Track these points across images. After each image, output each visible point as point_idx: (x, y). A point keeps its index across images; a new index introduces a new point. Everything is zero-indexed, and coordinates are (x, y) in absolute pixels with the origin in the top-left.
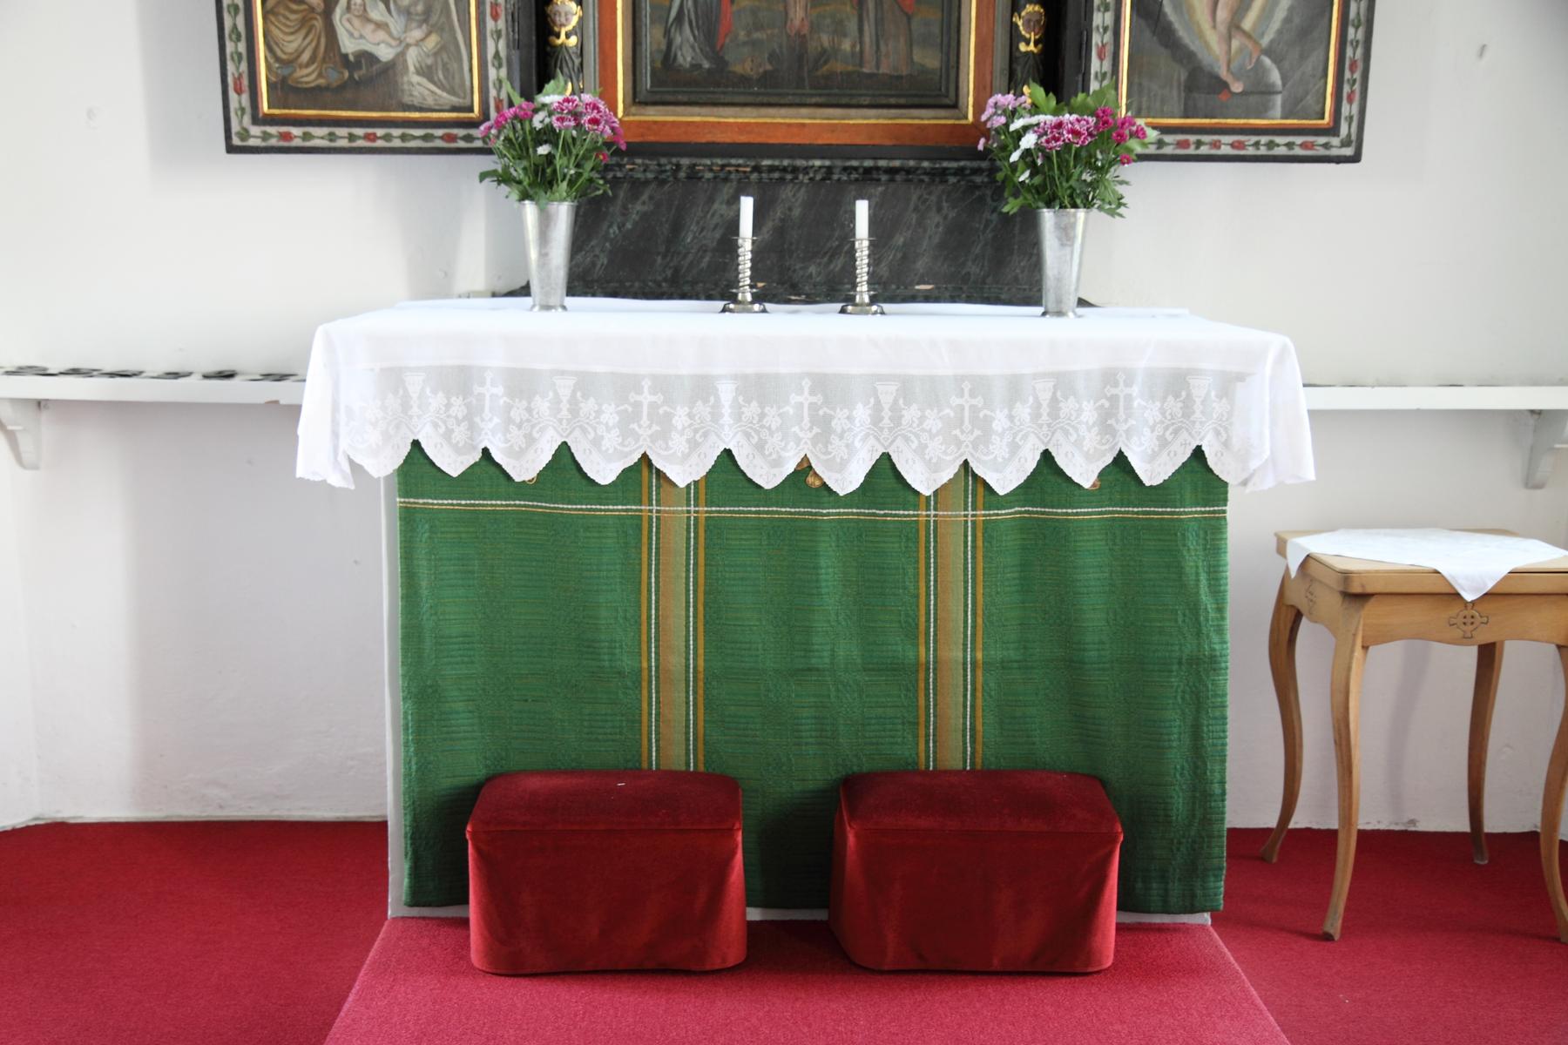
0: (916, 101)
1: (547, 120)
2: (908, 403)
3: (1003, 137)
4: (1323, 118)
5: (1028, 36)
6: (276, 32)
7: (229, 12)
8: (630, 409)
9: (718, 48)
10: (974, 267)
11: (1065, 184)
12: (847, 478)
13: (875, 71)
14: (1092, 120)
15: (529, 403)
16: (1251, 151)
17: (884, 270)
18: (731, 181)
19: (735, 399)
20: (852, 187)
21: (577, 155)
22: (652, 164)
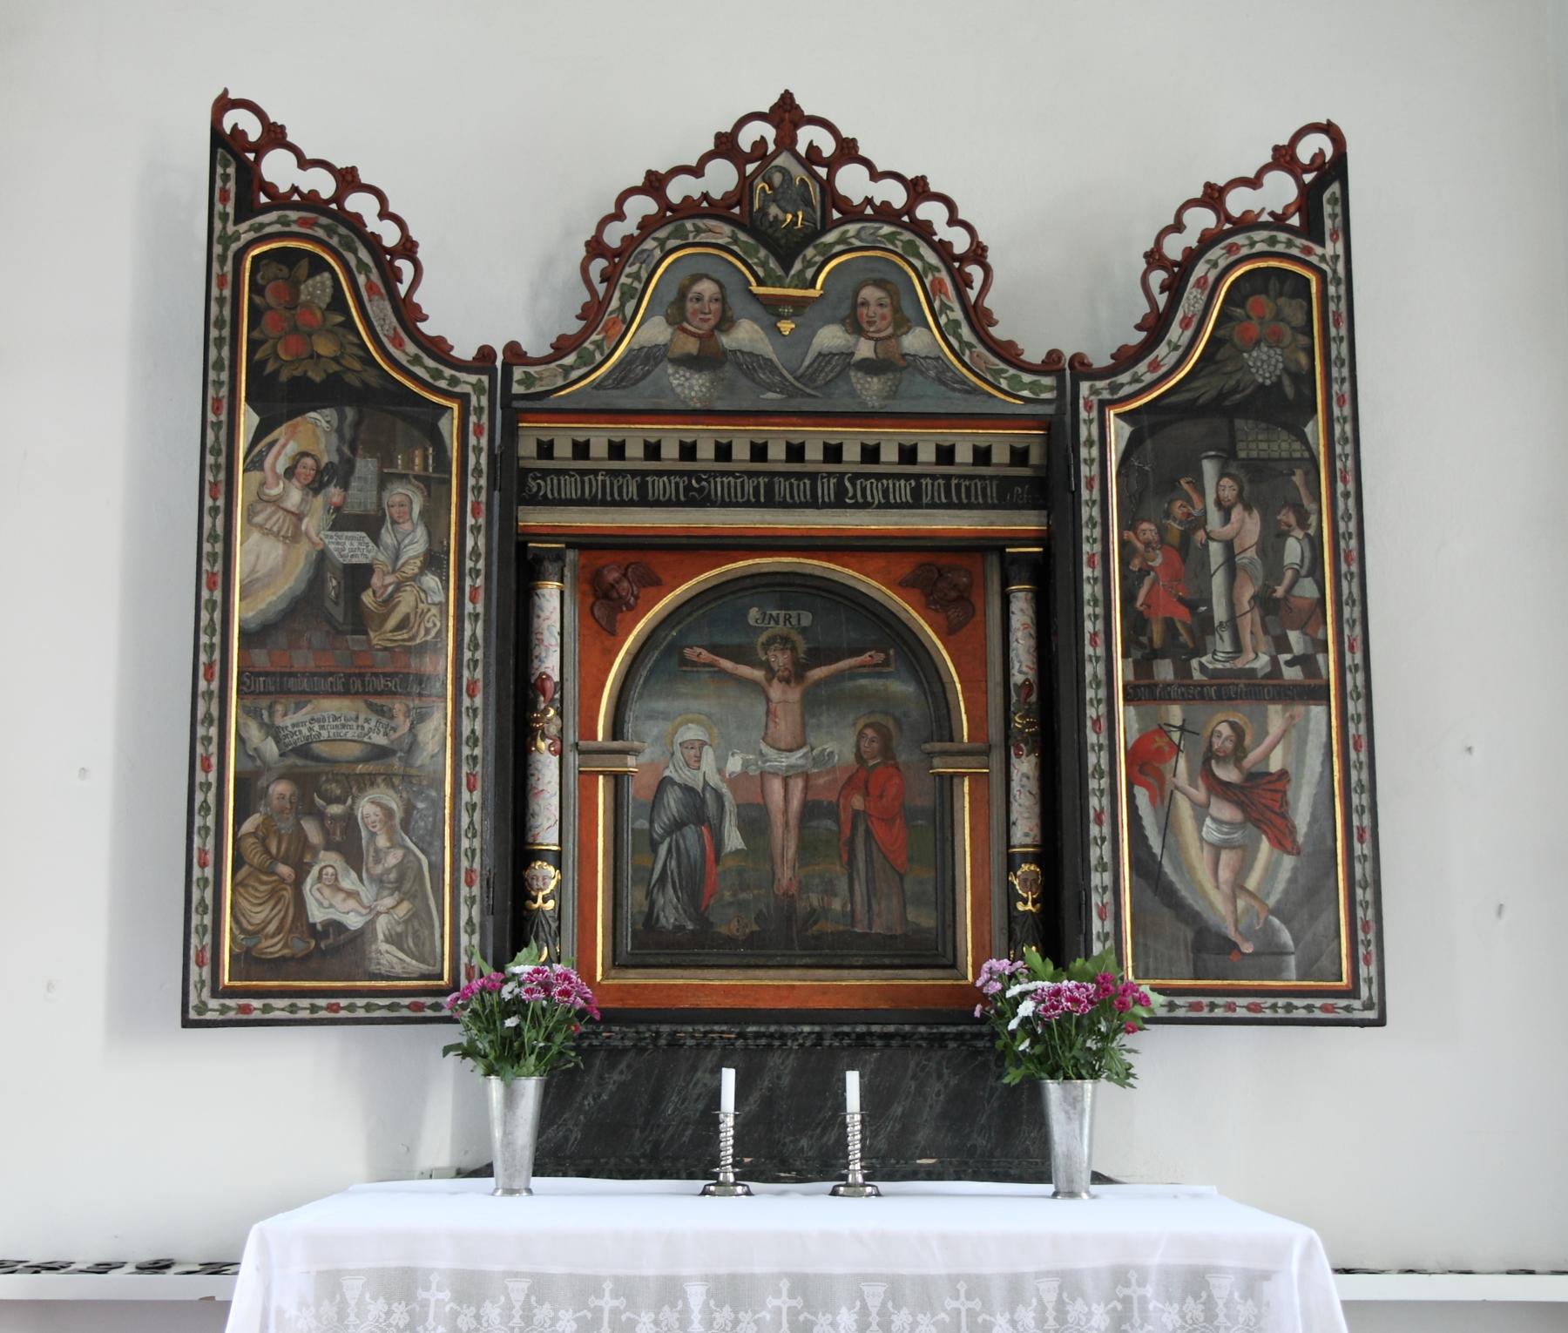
0: (912, 961)
1: (517, 990)
2: (897, 1307)
3: (999, 1004)
4: (1341, 980)
5: (1025, 895)
6: (244, 903)
7: (198, 885)
8: (589, 1316)
9: (703, 908)
10: (979, 1139)
11: (1067, 1054)
13: (868, 931)
14: (1092, 987)
15: (478, 1309)
16: (1268, 1014)
17: (882, 1144)
18: (715, 1047)
19: (706, 1303)
20: (845, 1053)
21: (547, 1027)
22: (630, 1031)
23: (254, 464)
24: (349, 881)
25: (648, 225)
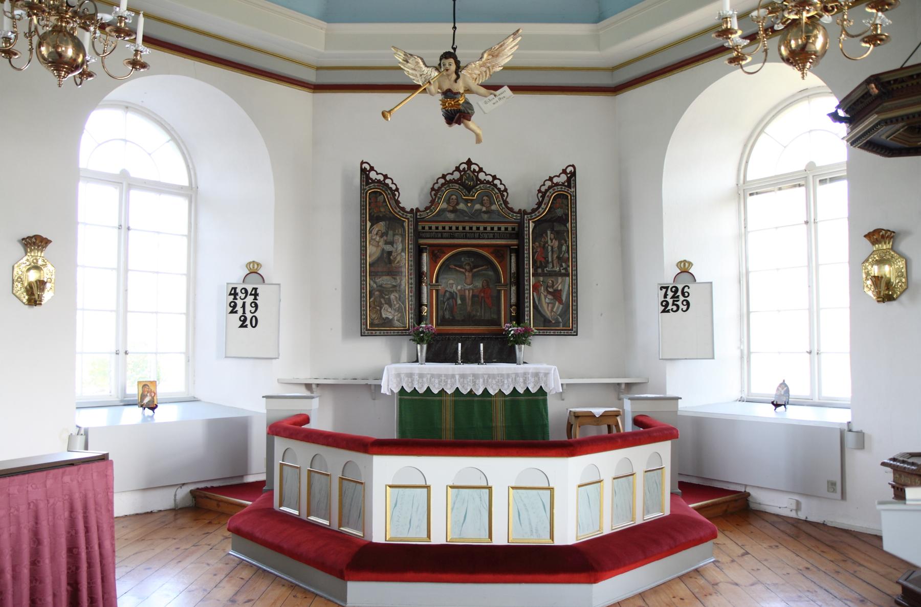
12: (479, 392)
16: (557, 334)
23: (370, 232)
24: (390, 310)
25: (443, 185)
